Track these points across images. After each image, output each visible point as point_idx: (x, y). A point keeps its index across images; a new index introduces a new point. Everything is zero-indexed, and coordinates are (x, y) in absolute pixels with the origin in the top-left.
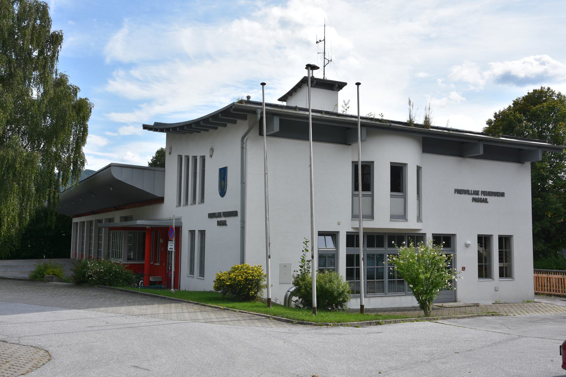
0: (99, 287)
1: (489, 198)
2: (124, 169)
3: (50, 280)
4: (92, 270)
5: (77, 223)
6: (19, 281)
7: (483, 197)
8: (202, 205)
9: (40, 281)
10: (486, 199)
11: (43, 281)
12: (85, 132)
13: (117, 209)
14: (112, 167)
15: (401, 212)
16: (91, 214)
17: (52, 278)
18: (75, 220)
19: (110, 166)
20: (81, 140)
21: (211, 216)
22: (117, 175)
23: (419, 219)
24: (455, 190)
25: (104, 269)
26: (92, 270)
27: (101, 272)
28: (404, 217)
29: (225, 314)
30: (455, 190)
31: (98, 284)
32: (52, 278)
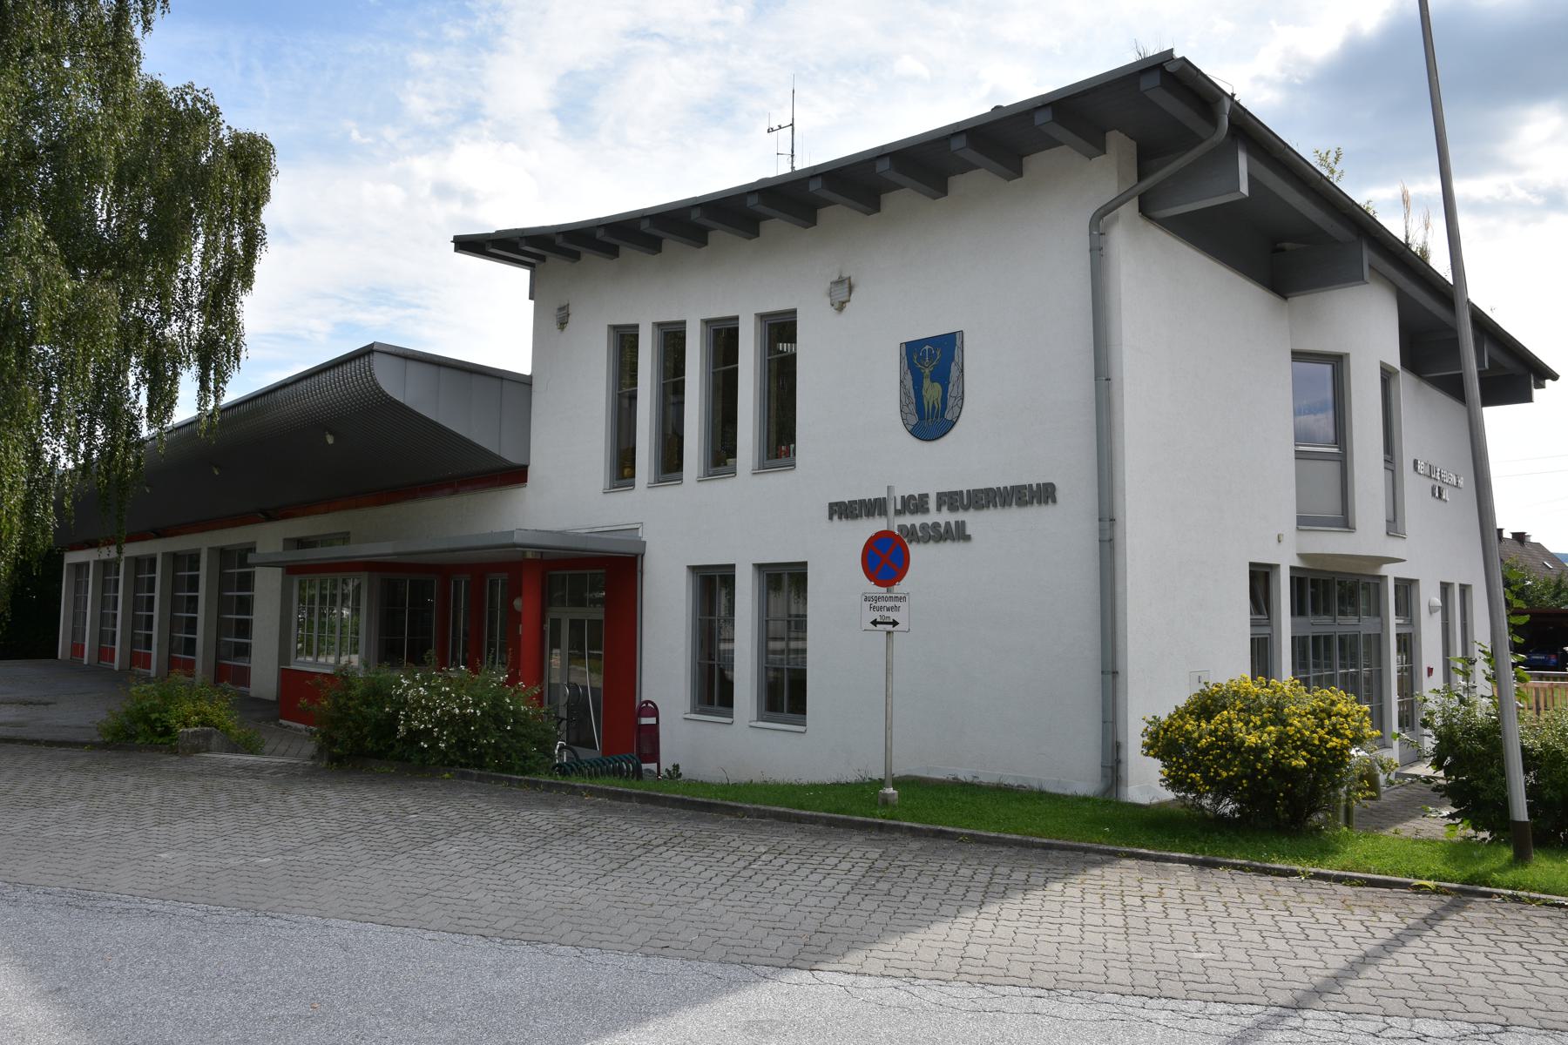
0: (463, 776)
1: (974, 520)
2: (412, 365)
3: (199, 746)
4: (431, 710)
5: (80, 568)
6: (58, 751)
7: (945, 517)
8: (777, 480)
9: (154, 748)
10: (961, 525)
11: (174, 751)
12: (253, 241)
13: (270, 516)
14: (376, 358)
15: (1331, 507)
16: (151, 538)
17: (207, 736)
18: (72, 558)
19: (368, 352)
20: (236, 272)
21: (842, 511)
22: (389, 381)
23: (1394, 527)
24: (831, 505)
25: (476, 705)
26: (431, 710)
27: (467, 720)
28: (1345, 522)
29: (540, 817)
30: (831, 505)
31: (452, 764)
32: (207, 736)
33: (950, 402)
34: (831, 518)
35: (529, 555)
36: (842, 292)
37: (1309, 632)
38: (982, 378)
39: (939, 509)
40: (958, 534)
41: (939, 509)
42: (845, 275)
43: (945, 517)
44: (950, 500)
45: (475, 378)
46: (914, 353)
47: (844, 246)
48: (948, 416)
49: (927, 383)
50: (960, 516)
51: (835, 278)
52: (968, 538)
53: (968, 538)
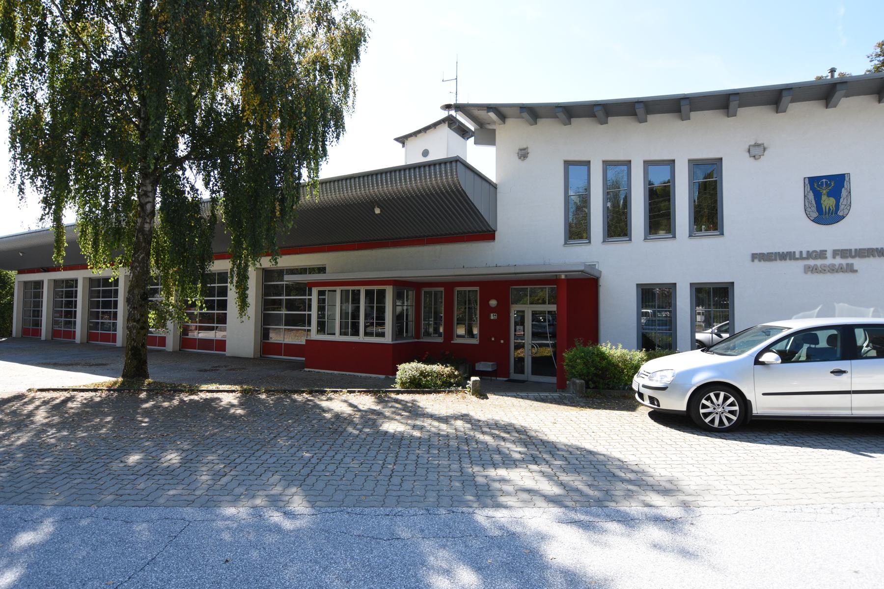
1: (857, 263)
33: (842, 207)
34: (753, 261)
35: (563, 277)
36: (756, 151)
37: (202, 206)
38: (860, 194)
39: (834, 257)
40: (851, 269)
41: (834, 257)
42: (759, 142)
43: (838, 261)
44: (844, 253)
45: (484, 182)
46: (814, 184)
47: (754, 123)
48: (840, 213)
49: (824, 198)
50: (850, 261)
51: (753, 143)
52: (397, 140)
53: (397, 140)
